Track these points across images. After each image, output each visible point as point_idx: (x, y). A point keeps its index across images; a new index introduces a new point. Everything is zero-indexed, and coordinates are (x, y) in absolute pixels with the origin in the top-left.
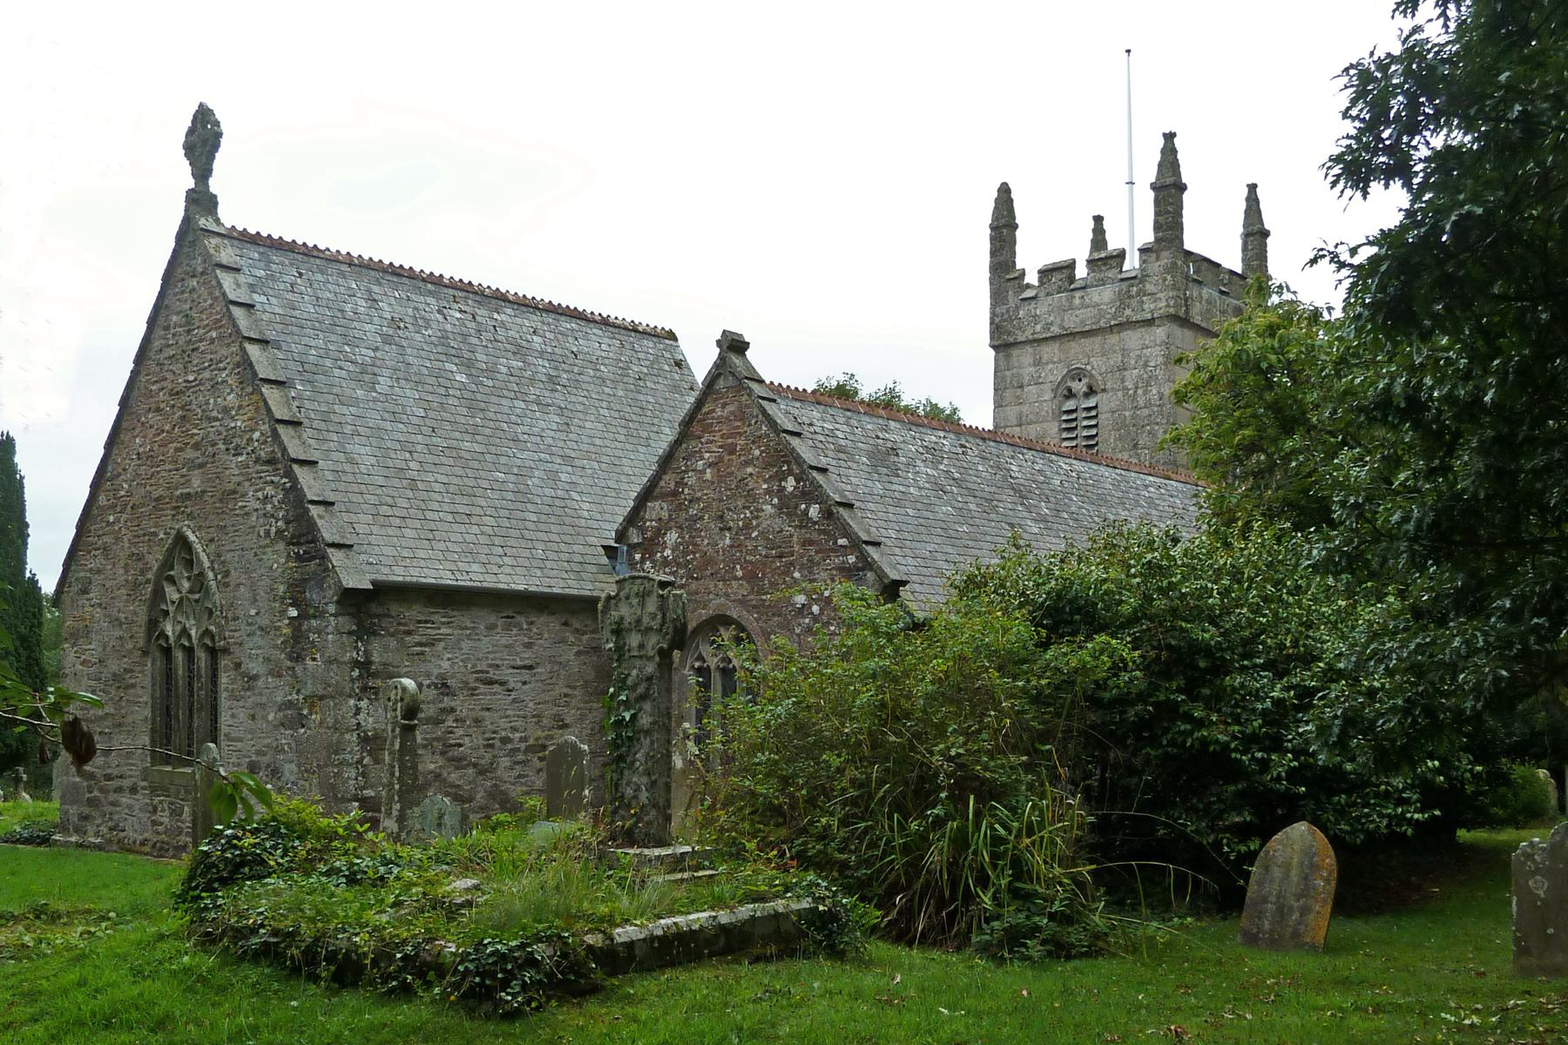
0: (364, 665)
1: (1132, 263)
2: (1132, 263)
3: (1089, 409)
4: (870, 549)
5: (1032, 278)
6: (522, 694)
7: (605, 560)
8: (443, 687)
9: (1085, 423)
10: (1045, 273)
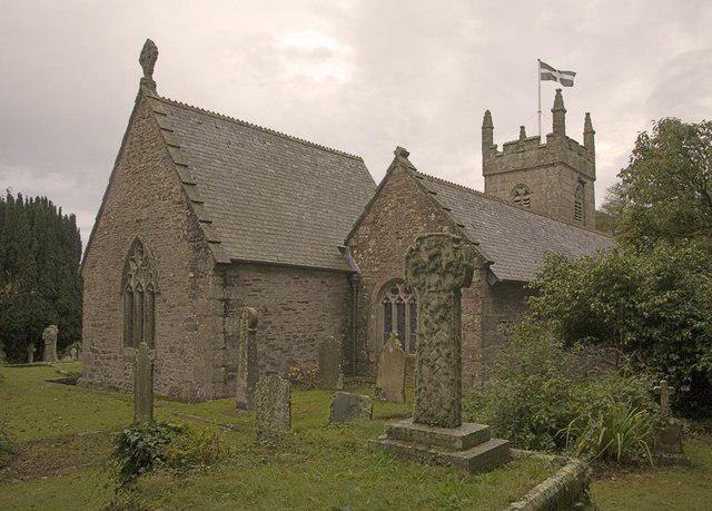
2: (544, 141)
5: (500, 149)
6: (306, 317)
7: (339, 253)
8: (266, 311)
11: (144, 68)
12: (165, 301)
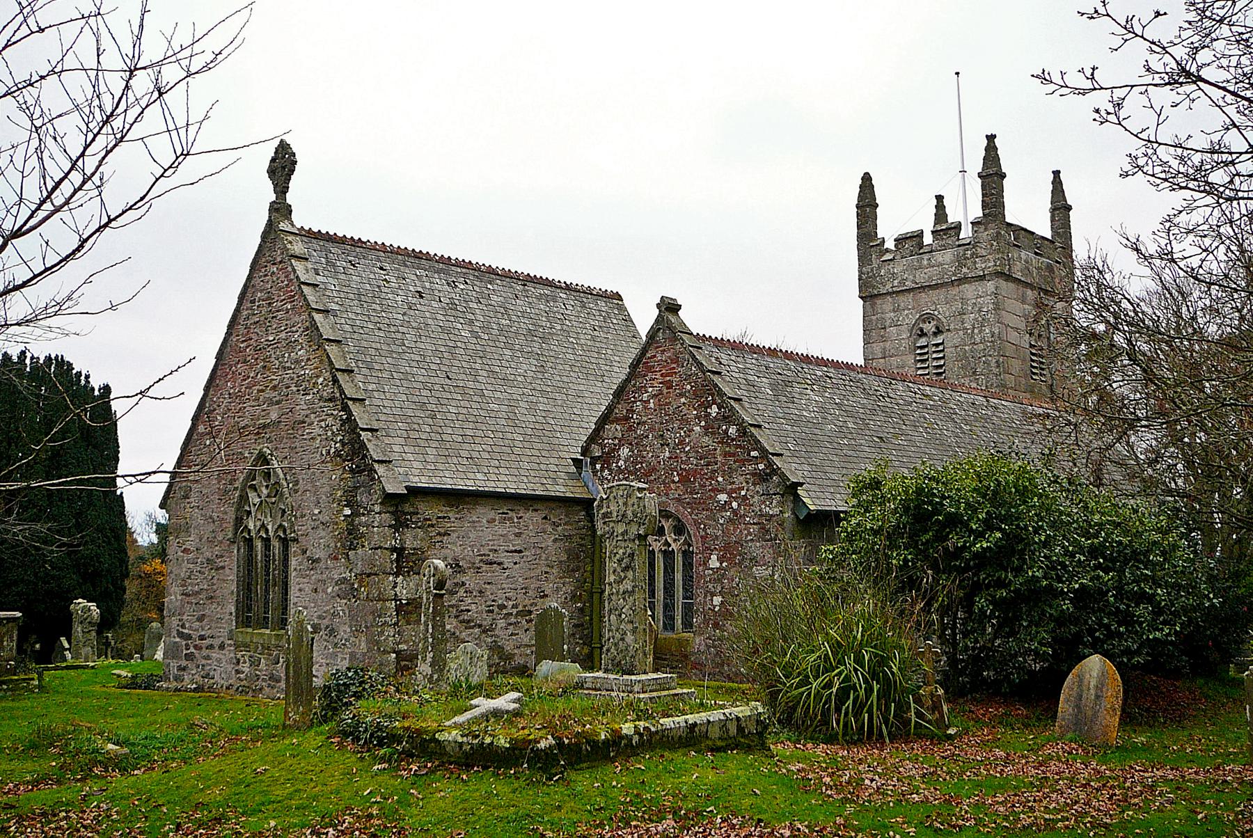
0: (400, 551)
1: (966, 233)
3: (937, 345)
4: (774, 458)
5: (890, 244)
6: (513, 567)
9: (935, 356)
10: (900, 241)
11: (275, 186)
12: (304, 552)
